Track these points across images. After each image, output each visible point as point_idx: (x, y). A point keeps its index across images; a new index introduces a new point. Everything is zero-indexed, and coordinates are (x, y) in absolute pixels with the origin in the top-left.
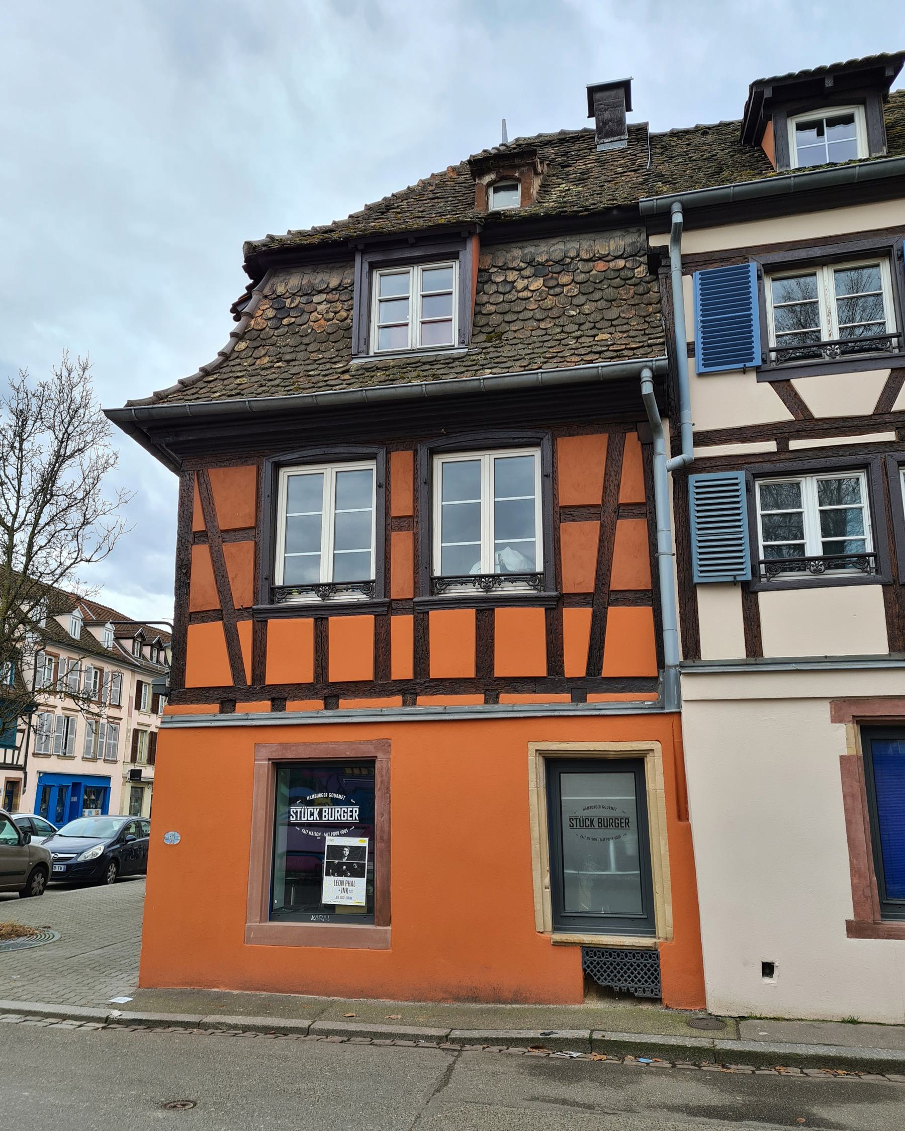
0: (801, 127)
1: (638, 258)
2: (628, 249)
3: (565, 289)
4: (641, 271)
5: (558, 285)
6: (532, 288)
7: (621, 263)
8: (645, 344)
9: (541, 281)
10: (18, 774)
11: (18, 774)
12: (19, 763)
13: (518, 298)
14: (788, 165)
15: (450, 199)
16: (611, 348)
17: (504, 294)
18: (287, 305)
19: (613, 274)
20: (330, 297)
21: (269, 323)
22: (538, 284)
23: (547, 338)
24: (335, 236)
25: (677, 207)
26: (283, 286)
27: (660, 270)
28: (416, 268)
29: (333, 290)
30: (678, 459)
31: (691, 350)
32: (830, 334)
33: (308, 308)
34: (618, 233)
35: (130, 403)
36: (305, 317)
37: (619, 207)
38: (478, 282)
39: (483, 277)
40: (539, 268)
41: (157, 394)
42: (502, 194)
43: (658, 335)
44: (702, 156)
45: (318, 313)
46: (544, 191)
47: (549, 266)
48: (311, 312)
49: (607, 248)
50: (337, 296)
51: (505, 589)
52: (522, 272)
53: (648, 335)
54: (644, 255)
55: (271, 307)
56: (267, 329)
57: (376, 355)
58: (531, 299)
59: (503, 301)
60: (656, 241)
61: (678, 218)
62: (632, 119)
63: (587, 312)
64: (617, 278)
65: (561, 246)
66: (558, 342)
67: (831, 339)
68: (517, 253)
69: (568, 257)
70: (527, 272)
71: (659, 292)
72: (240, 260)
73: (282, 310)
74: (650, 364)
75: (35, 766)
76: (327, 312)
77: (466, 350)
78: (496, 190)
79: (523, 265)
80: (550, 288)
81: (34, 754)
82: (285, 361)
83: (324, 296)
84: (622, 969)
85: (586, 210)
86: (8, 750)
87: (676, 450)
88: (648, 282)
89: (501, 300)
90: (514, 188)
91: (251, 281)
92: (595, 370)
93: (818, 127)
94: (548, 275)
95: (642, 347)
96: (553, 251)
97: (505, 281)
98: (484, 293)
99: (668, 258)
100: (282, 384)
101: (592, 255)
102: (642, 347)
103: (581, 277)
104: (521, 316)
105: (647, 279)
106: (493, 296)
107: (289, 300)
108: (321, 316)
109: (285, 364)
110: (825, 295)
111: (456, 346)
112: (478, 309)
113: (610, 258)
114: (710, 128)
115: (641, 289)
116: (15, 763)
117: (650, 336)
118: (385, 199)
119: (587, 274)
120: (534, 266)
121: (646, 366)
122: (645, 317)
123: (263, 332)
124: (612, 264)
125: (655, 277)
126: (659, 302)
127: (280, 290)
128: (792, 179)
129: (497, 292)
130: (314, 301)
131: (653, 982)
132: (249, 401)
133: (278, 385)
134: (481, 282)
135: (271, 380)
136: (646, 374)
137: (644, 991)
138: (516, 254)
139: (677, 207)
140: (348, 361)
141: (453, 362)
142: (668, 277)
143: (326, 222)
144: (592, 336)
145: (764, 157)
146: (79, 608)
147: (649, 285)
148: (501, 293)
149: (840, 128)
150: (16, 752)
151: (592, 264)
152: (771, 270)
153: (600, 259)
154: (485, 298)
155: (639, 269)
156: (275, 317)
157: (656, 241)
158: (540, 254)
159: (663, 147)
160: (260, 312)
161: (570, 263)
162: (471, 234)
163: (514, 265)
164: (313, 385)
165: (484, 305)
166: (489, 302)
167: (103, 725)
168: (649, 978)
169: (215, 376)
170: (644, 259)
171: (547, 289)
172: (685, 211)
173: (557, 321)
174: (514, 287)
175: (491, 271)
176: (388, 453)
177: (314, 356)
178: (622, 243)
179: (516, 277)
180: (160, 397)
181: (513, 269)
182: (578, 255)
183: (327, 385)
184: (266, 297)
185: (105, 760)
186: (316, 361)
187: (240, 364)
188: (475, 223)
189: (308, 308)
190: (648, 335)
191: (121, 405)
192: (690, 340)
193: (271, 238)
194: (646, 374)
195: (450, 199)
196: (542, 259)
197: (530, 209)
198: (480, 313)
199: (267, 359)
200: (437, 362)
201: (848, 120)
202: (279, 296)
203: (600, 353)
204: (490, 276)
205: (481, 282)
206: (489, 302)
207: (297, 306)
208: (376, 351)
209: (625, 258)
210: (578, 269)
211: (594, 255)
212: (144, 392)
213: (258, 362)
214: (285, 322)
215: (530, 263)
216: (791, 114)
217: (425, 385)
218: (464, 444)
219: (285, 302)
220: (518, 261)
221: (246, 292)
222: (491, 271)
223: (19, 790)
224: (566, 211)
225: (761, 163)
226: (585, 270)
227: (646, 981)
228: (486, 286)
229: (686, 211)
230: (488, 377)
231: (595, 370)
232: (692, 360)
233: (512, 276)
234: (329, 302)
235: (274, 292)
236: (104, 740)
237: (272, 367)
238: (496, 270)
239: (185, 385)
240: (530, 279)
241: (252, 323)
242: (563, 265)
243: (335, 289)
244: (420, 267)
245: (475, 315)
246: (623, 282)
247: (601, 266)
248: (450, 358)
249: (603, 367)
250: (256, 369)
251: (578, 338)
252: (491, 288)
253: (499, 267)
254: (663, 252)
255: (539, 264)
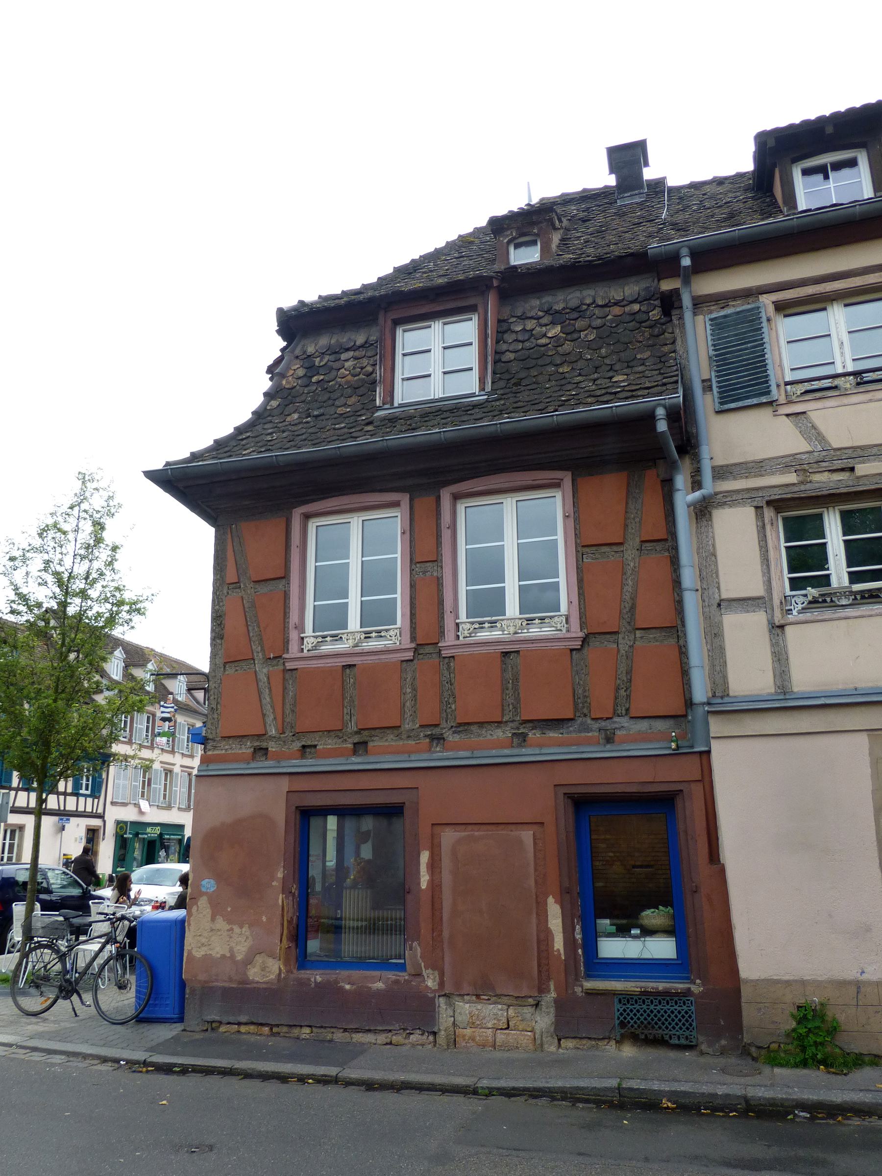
0: (806, 172)
1: (652, 302)
2: (643, 293)
3: (582, 334)
4: (655, 314)
5: (575, 331)
6: (550, 335)
7: (636, 307)
8: (660, 383)
9: (559, 328)
10: (95, 822)
11: (95, 822)
12: (99, 812)
13: (537, 345)
14: (796, 207)
15: (474, 257)
16: (626, 389)
17: (523, 342)
18: (317, 364)
19: (628, 318)
20: (357, 354)
21: (300, 381)
22: (555, 331)
23: (563, 382)
24: (361, 297)
25: (685, 251)
26: (313, 346)
27: (674, 312)
28: (437, 322)
29: (360, 347)
30: (697, 494)
31: (707, 386)
32: (844, 366)
33: (336, 365)
34: (633, 279)
35: (168, 464)
36: (334, 373)
37: (632, 255)
38: (497, 332)
39: (503, 328)
40: (556, 317)
41: (192, 454)
42: (523, 250)
43: (672, 374)
44: (717, 204)
45: (345, 369)
46: (564, 244)
47: (567, 313)
48: (339, 369)
49: (622, 294)
50: (364, 352)
51: (531, 630)
52: (540, 320)
53: (663, 374)
54: (657, 299)
55: (302, 366)
56: (298, 387)
57: (401, 406)
58: (550, 346)
59: (522, 349)
60: (667, 286)
61: (686, 262)
62: (649, 174)
63: (604, 355)
64: (632, 321)
65: (578, 294)
66: (576, 385)
67: (845, 371)
68: (536, 302)
69: (584, 305)
70: (545, 321)
71: (673, 333)
72: (273, 324)
73: (312, 369)
74: (663, 402)
75: (114, 814)
76: (354, 368)
77: (486, 397)
78: (517, 246)
79: (540, 314)
80: (567, 334)
81: (113, 803)
82: (314, 416)
83: (351, 354)
84: (655, 1016)
85: (599, 260)
86: (88, 799)
87: (697, 484)
88: (663, 324)
89: (520, 347)
90: (534, 243)
91: (285, 344)
92: (609, 411)
93: (823, 171)
94: (565, 322)
95: (657, 386)
96: (569, 300)
97: (524, 330)
98: (504, 342)
99: (680, 300)
100: (310, 438)
101: (607, 301)
102: (657, 386)
103: (599, 322)
104: (540, 362)
105: (662, 321)
106: (513, 344)
107: (318, 359)
108: (348, 372)
109: (314, 418)
110: (837, 328)
111: (477, 394)
112: (497, 357)
113: (625, 303)
114: (726, 178)
115: (656, 331)
116: (94, 811)
117: (665, 375)
118: (413, 261)
119: (604, 320)
120: (552, 314)
121: (659, 405)
122: (660, 357)
123: (293, 390)
124: (627, 309)
125: (669, 319)
126: (674, 343)
127: (311, 349)
128: (795, 220)
129: (516, 340)
130: (342, 359)
131: (688, 1029)
132: (276, 456)
133: (305, 440)
134: (500, 332)
135: (299, 435)
136: (660, 412)
137: (679, 1038)
138: (534, 305)
139: (685, 251)
140: (373, 413)
141: (473, 409)
142: (681, 318)
143: (355, 284)
144: (608, 378)
145: (774, 203)
146: (153, 661)
147: (664, 327)
148: (520, 341)
149: (846, 172)
150: (96, 801)
151: (608, 309)
152: (783, 308)
153: (615, 304)
154: (504, 347)
155: (653, 312)
156: (305, 375)
157: (667, 286)
158: (557, 303)
159: (680, 198)
160: (291, 372)
161: (586, 310)
162: (489, 287)
163: (532, 314)
164: (337, 437)
165: (503, 353)
166: (508, 350)
167: (177, 774)
168: (684, 1025)
169: (248, 434)
170: (657, 303)
171: (564, 336)
172: (693, 255)
173: (574, 365)
174: (532, 335)
175: (510, 321)
176: (411, 500)
177: (340, 410)
178: (636, 288)
179: (535, 326)
180: (195, 456)
181: (532, 318)
182: (594, 302)
183: (352, 437)
184: (297, 357)
185: (179, 808)
186: (342, 414)
187: (271, 422)
188: (491, 278)
189: (336, 365)
190: (663, 374)
191: (159, 466)
192: (706, 376)
193: (301, 302)
194: (660, 412)
195: (474, 257)
196: (559, 307)
197: (547, 262)
198: (500, 360)
199: (296, 416)
200: (458, 409)
201: (852, 163)
202: (309, 356)
203: (615, 393)
204: (510, 326)
205: (500, 332)
206: (508, 350)
207: (326, 364)
208: (400, 402)
209: (640, 303)
210: (594, 314)
211: (610, 301)
212: (180, 453)
213: (288, 419)
214: (314, 379)
215: (547, 312)
216: (795, 160)
217: (444, 432)
218: (333, 509)
219: (315, 361)
220: (536, 310)
221: (280, 354)
222: (510, 321)
223: (98, 838)
224: (580, 262)
225: (770, 208)
226: (600, 315)
227: (681, 1028)
228: (506, 336)
229: (694, 254)
230: (507, 422)
231: (609, 411)
232: (708, 397)
233: (530, 324)
234: (356, 358)
235: (305, 352)
236: (178, 789)
237: (299, 423)
238: (515, 319)
239: (220, 445)
240: (548, 327)
241: (284, 382)
242: (580, 312)
243: (362, 346)
244: (441, 321)
245: (495, 363)
246: (638, 325)
247: (617, 310)
248: (469, 406)
249: (620, 406)
250: (287, 426)
251: (595, 380)
252: (509, 337)
253: (518, 317)
254: (676, 293)
255: (557, 312)
